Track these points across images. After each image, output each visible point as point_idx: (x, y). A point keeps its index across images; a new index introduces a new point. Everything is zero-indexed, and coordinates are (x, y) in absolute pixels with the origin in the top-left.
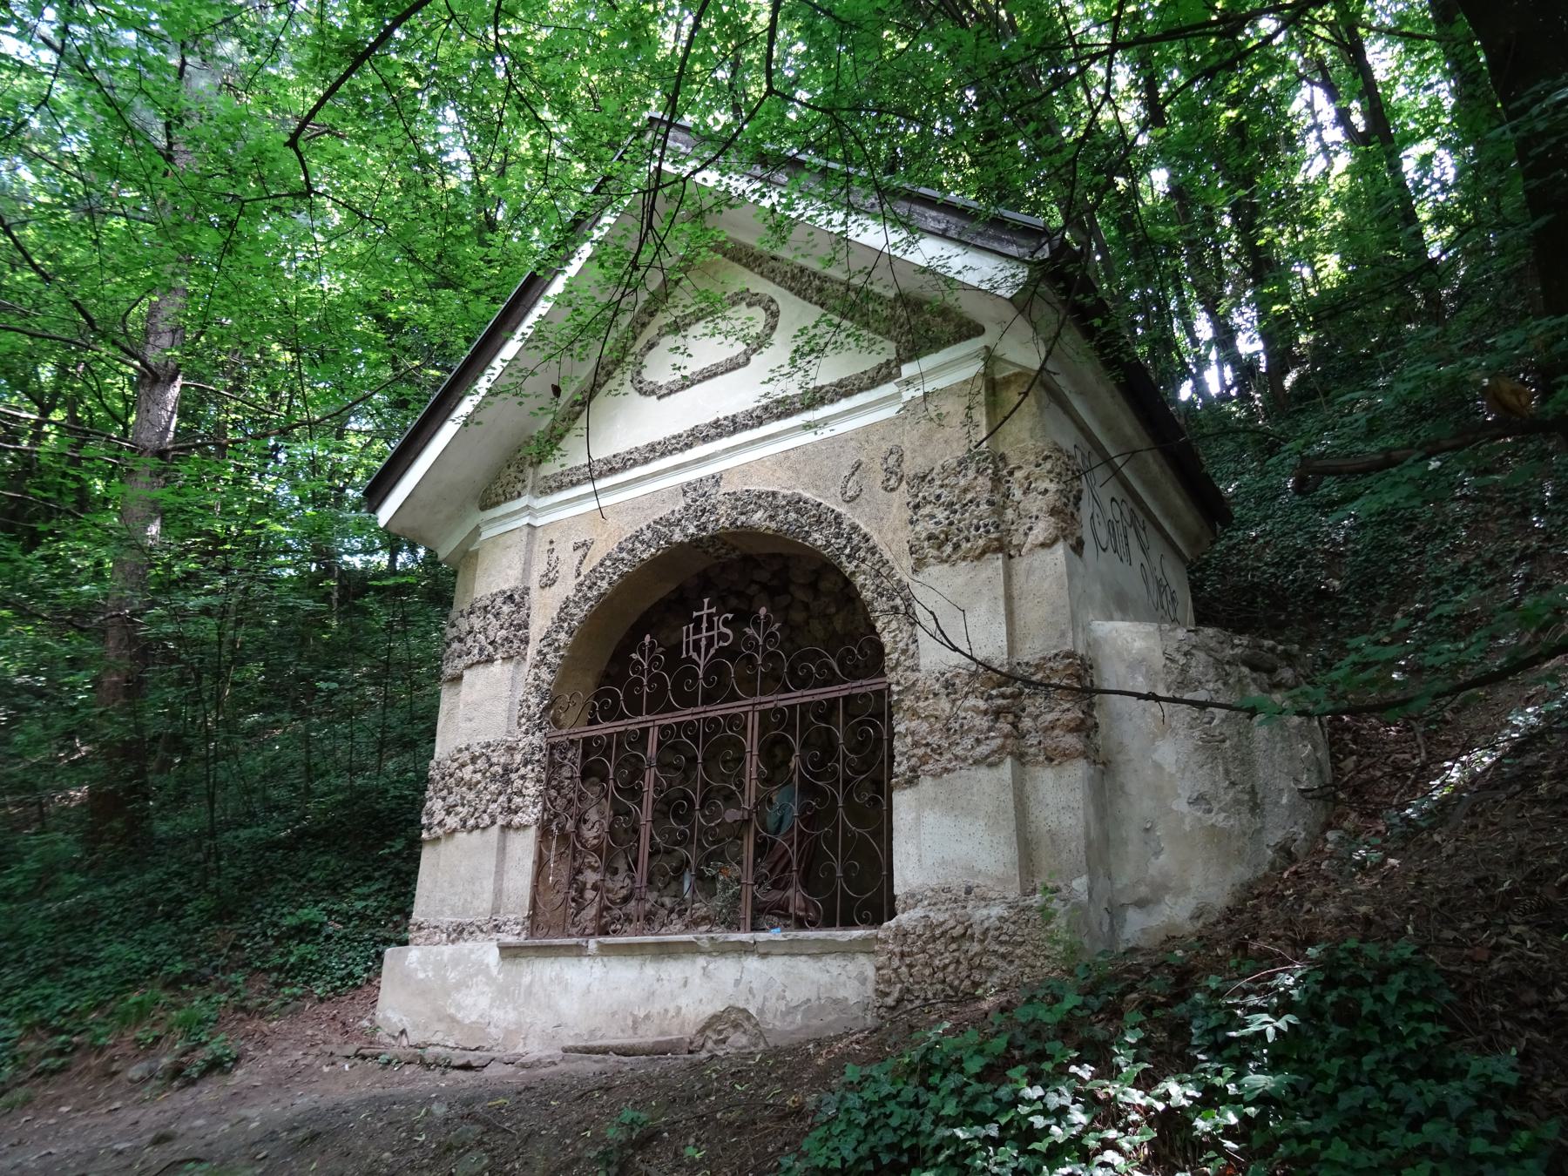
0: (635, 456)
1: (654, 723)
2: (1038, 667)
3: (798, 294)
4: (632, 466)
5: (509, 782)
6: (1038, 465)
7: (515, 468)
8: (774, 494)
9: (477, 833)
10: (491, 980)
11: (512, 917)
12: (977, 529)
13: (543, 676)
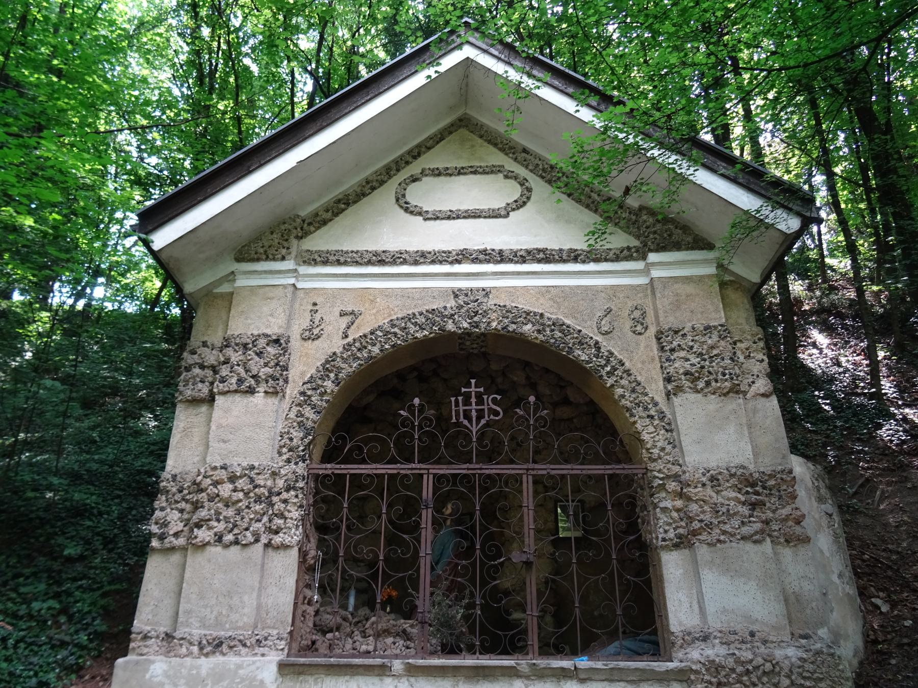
1: (429, 473)
2: (771, 476)
4: (402, 264)
5: (272, 505)
6: (755, 343)
7: (278, 234)
8: (542, 315)
9: (235, 549)
11: (275, 632)
12: (724, 375)
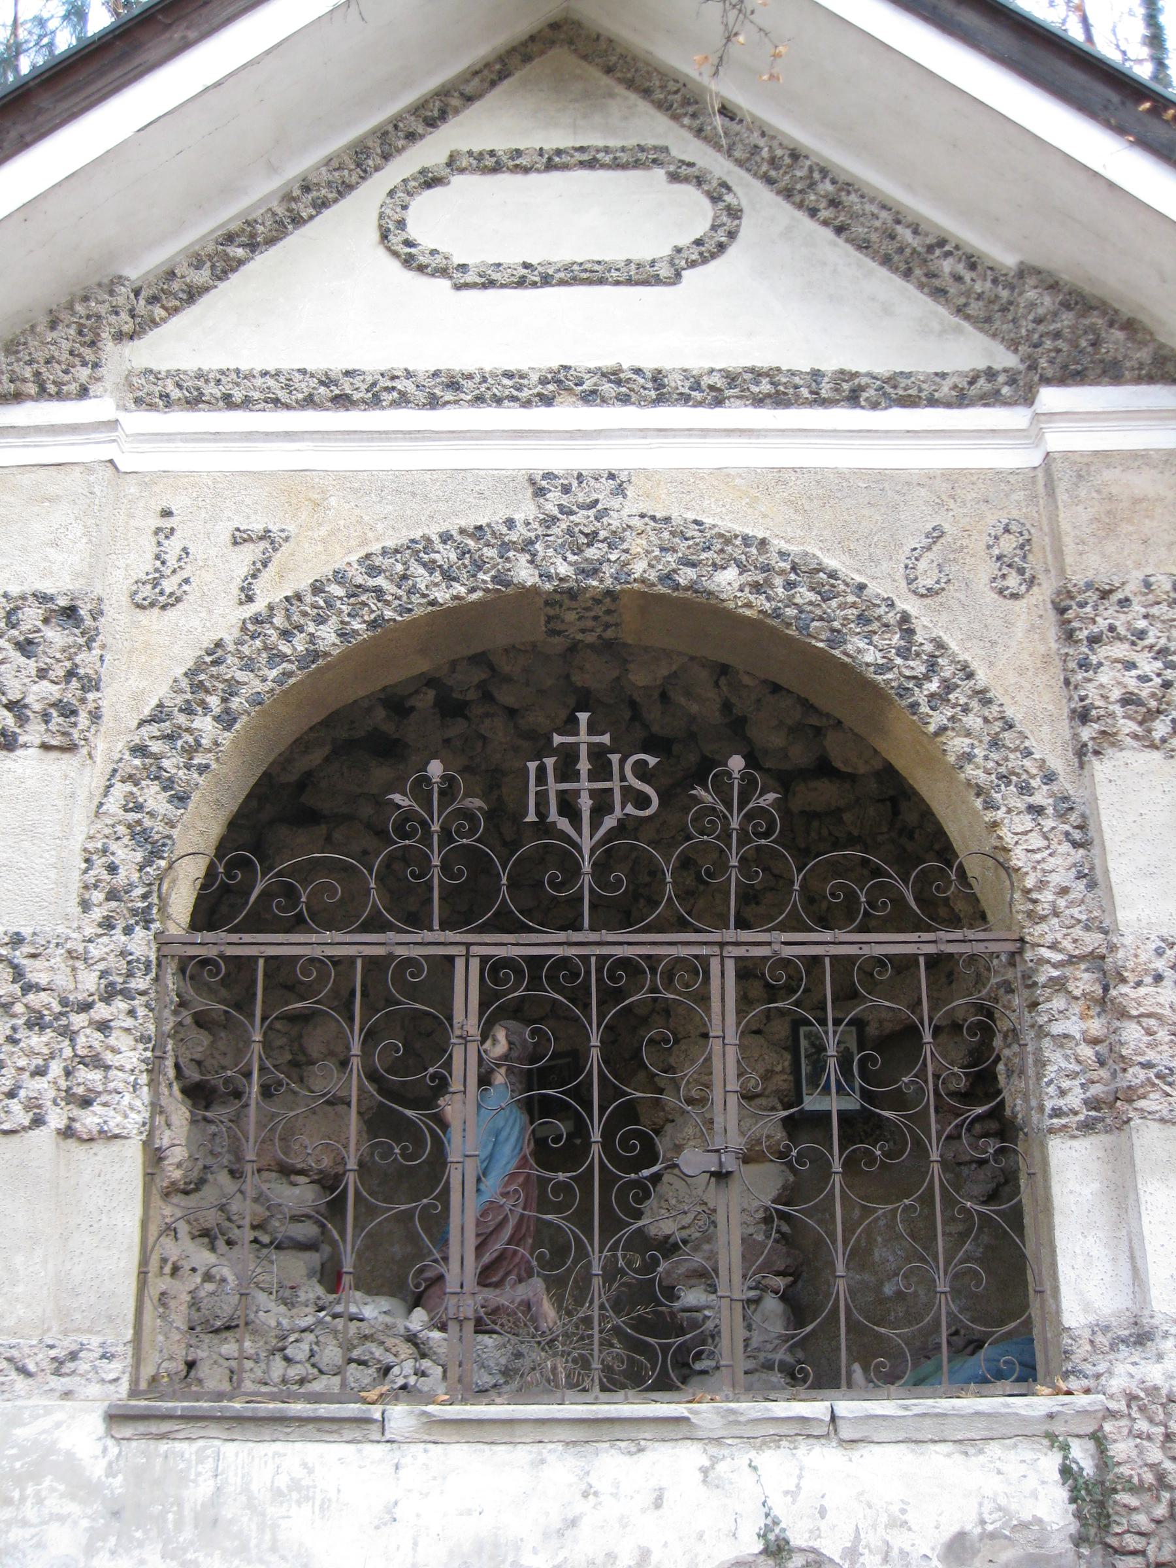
0: (407, 385)
3: (787, 193)
10: (80, 1487)
13: (151, 805)
